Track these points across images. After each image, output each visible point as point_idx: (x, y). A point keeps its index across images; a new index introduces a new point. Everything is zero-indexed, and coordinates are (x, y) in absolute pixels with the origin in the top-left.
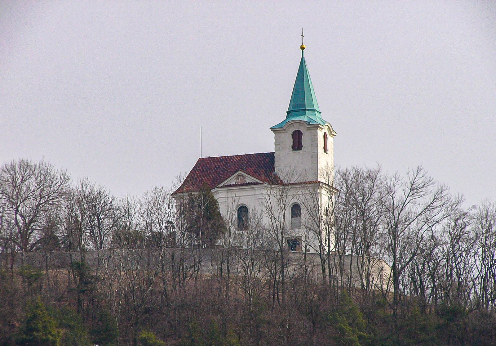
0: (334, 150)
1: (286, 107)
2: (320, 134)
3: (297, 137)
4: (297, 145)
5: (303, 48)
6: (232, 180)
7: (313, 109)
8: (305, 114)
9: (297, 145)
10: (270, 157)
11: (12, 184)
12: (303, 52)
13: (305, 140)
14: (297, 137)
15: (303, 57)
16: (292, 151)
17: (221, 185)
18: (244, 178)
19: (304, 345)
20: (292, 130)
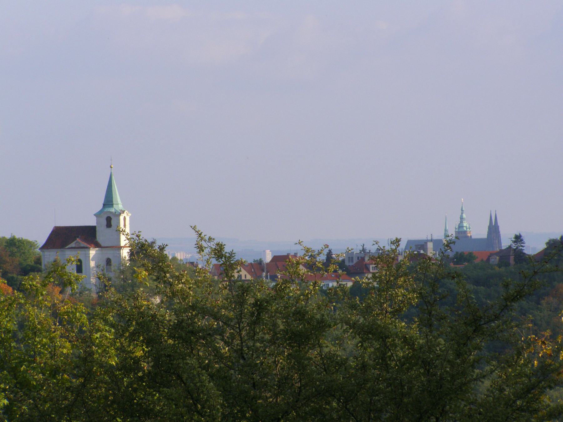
2: (122, 218)
3: (109, 220)
4: (109, 225)
6: (73, 245)
8: (113, 207)
9: (109, 225)
13: (113, 222)
14: (109, 220)
20: (106, 216)
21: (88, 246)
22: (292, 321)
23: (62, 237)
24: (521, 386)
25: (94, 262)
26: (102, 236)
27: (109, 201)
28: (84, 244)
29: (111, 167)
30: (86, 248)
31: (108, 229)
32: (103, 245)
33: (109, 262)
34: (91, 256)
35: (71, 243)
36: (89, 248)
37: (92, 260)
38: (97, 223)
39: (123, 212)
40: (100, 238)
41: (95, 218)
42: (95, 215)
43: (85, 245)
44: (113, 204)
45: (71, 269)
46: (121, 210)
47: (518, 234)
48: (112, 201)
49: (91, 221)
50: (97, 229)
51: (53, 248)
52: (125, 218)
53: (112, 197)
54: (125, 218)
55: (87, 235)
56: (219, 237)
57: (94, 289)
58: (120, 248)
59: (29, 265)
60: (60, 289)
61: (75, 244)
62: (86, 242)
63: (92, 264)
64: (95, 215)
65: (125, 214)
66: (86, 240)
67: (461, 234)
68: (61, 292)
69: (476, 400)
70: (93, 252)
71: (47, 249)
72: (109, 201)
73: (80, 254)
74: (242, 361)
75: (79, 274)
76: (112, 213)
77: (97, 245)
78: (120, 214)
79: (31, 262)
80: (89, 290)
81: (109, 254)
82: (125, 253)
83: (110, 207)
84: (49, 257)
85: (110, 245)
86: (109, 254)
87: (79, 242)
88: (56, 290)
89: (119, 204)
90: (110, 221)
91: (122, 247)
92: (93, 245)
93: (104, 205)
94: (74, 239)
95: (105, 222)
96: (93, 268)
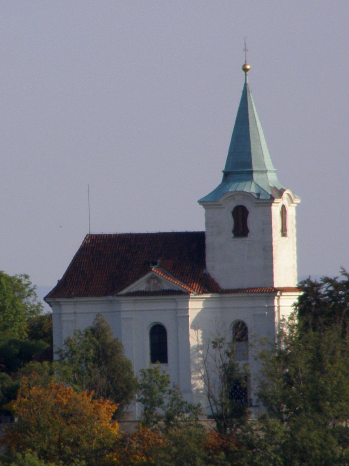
0: (299, 226)
1: (222, 165)
2: (276, 209)
3: (240, 216)
4: (241, 228)
5: (245, 50)
6: (140, 285)
7: (264, 169)
8: (251, 179)
9: (241, 228)
10: (198, 239)
11: (31, 455)
12: (246, 75)
13: (252, 222)
14: (240, 216)
15: (246, 84)
16: (233, 238)
17: (124, 291)
18: (159, 281)
19: (265, 465)
20: (232, 205)
21: (184, 287)
22: (166, 431)
23: (109, 264)
24: (262, 434)
25: (200, 332)
26: (219, 262)
27: (240, 163)
28: (170, 282)
29: (245, 70)
31: (239, 240)
32: (223, 285)
33: (240, 331)
35: (137, 278)
36: (187, 293)
37: (195, 328)
38: (206, 229)
39: (280, 193)
40: (215, 266)
41: (201, 210)
42: (201, 202)
44: (251, 173)
45: (136, 351)
46: (275, 188)
48: (250, 165)
49: (193, 221)
50: (209, 241)
51: (86, 295)
52: (284, 211)
53: (250, 154)
54: (284, 211)
57: (204, 403)
58: (272, 292)
59: (14, 342)
60: (114, 408)
61: (148, 282)
62: (176, 277)
63: (195, 338)
64: (201, 202)
65: (284, 200)
66: (177, 272)
68: (116, 416)
70: (196, 305)
71: (69, 296)
72: (240, 163)
73: (157, 311)
74: (241, 405)
75: (158, 365)
76: (248, 195)
77: (208, 286)
78: (272, 199)
79: (19, 332)
80: (194, 409)
81: (241, 309)
82: (286, 306)
83: (241, 180)
84: (75, 320)
86: (241, 309)
87: (159, 276)
88: (103, 409)
89: (268, 172)
91: (276, 290)
92: (196, 286)
93: (227, 175)
94: (145, 269)
95: (229, 222)
96: (199, 347)
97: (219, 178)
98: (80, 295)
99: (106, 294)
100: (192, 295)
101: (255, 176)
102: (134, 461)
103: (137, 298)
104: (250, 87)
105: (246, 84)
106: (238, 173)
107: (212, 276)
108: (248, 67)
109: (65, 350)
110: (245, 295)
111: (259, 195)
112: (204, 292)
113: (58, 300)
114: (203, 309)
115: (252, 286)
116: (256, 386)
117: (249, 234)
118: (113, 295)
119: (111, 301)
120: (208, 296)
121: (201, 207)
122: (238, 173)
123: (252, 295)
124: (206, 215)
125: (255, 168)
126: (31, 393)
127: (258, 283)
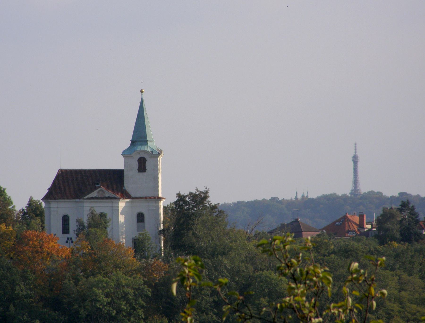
6: (94, 194)
8: (147, 144)
15: (142, 99)
18: (104, 192)
20: (138, 156)
23: (71, 184)
25: (124, 216)
26: (133, 182)
27: (140, 136)
28: (108, 193)
30: (115, 198)
31: (141, 174)
32: (133, 195)
33: (140, 218)
34: (120, 209)
36: (119, 199)
37: (122, 214)
40: (129, 185)
41: (122, 159)
43: (112, 195)
44: (147, 141)
47: (405, 200)
48: (145, 137)
49: (118, 164)
50: (125, 174)
55: (112, 181)
56: (209, 194)
61: (98, 193)
63: (122, 219)
67: (292, 199)
69: (264, 298)
70: (122, 204)
72: (140, 136)
73: (100, 207)
76: (147, 152)
77: (127, 195)
81: (142, 207)
83: (142, 145)
85: (144, 196)
86: (142, 207)
90: (144, 163)
93: (133, 142)
95: (136, 165)
97: (128, 144)
98: (60, 199)
99: (74, 198)
100: (121, 200)
101: (148, 143)
102: (272, 312)
103: (91, 200)
104: (145, 101)
105: (142, 99)
106: (140, 141)
107: (127, 191)
108: (143, 91)
109: (243, 272)
110: (144, 200)
111: (152, 152)
112: (126, 198)
113: (49, 201)
114: (125, 207)
115: (148, 196)
116: (273, 274)
117: (146, 171)
118: (80, 199)
119: (76, 202)
120: (128, 200)
121: (123, 157)
122: (140, 141)
123: (147, 200)
124: (125, 161)
125: (148, 139)
126: (367, 316)
127: (150, 194)
